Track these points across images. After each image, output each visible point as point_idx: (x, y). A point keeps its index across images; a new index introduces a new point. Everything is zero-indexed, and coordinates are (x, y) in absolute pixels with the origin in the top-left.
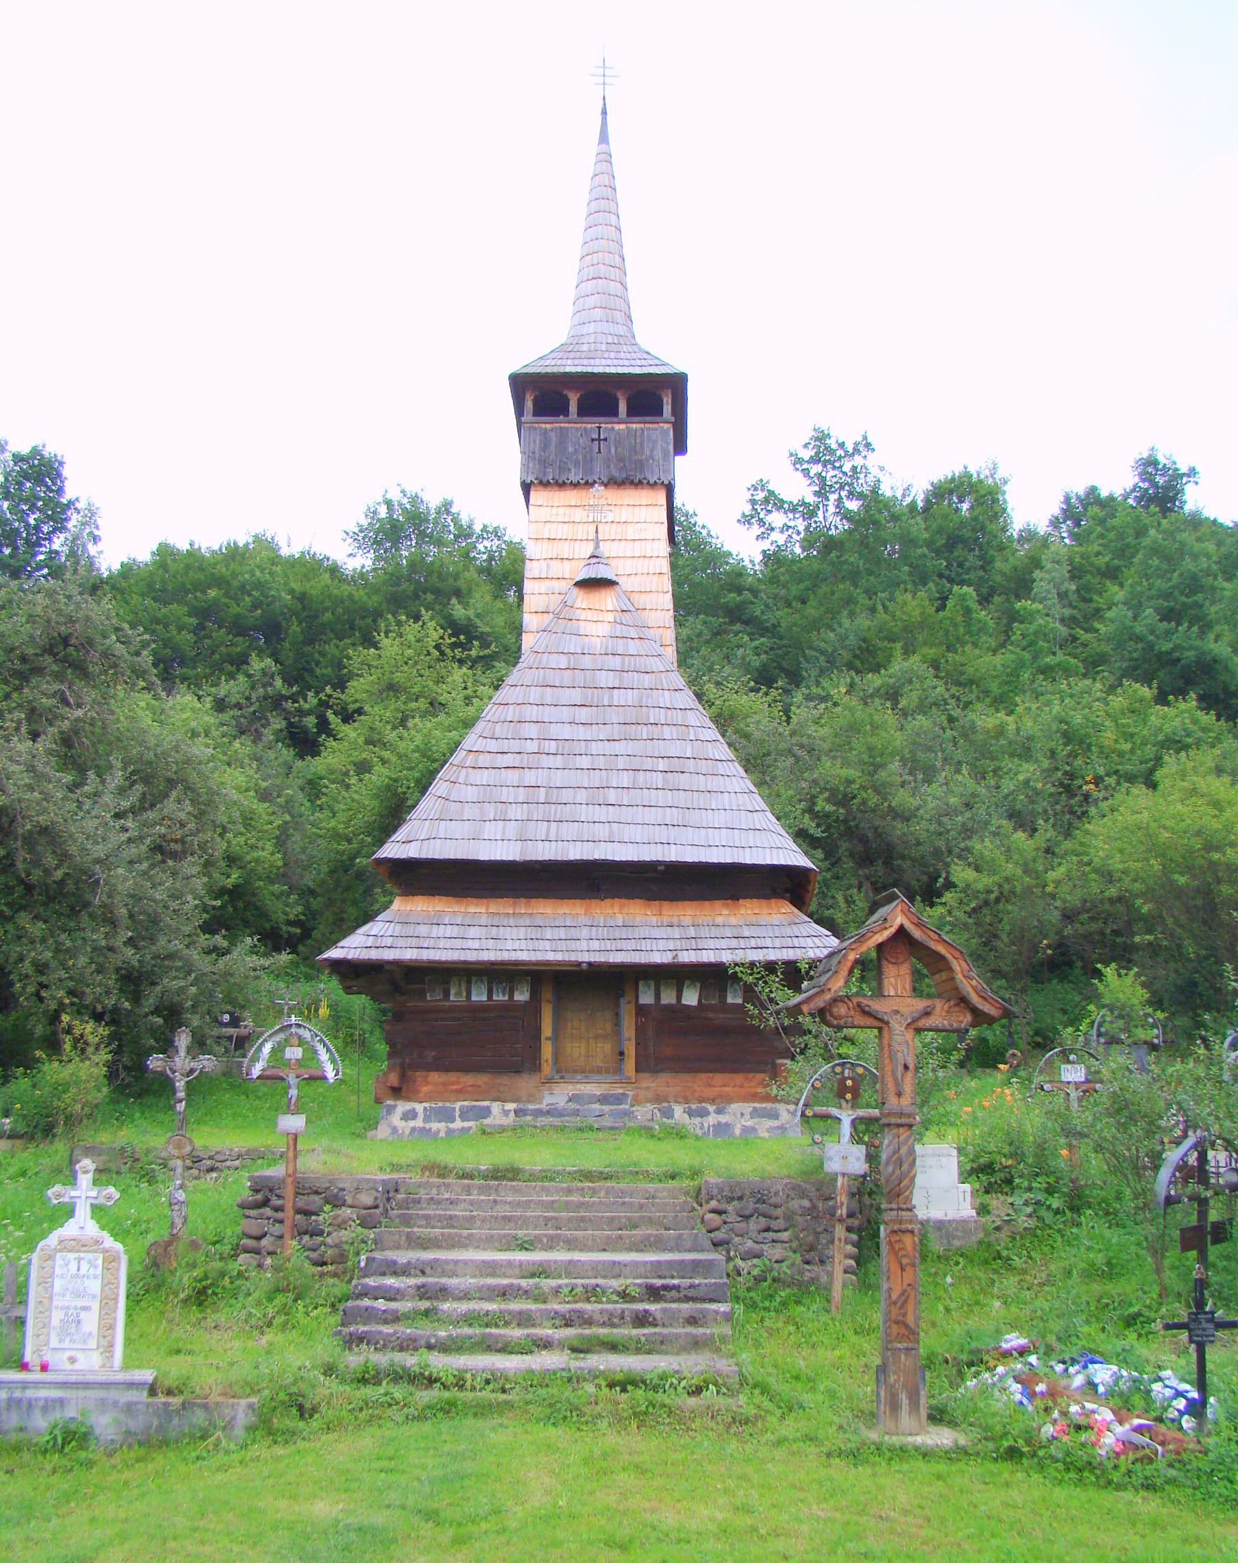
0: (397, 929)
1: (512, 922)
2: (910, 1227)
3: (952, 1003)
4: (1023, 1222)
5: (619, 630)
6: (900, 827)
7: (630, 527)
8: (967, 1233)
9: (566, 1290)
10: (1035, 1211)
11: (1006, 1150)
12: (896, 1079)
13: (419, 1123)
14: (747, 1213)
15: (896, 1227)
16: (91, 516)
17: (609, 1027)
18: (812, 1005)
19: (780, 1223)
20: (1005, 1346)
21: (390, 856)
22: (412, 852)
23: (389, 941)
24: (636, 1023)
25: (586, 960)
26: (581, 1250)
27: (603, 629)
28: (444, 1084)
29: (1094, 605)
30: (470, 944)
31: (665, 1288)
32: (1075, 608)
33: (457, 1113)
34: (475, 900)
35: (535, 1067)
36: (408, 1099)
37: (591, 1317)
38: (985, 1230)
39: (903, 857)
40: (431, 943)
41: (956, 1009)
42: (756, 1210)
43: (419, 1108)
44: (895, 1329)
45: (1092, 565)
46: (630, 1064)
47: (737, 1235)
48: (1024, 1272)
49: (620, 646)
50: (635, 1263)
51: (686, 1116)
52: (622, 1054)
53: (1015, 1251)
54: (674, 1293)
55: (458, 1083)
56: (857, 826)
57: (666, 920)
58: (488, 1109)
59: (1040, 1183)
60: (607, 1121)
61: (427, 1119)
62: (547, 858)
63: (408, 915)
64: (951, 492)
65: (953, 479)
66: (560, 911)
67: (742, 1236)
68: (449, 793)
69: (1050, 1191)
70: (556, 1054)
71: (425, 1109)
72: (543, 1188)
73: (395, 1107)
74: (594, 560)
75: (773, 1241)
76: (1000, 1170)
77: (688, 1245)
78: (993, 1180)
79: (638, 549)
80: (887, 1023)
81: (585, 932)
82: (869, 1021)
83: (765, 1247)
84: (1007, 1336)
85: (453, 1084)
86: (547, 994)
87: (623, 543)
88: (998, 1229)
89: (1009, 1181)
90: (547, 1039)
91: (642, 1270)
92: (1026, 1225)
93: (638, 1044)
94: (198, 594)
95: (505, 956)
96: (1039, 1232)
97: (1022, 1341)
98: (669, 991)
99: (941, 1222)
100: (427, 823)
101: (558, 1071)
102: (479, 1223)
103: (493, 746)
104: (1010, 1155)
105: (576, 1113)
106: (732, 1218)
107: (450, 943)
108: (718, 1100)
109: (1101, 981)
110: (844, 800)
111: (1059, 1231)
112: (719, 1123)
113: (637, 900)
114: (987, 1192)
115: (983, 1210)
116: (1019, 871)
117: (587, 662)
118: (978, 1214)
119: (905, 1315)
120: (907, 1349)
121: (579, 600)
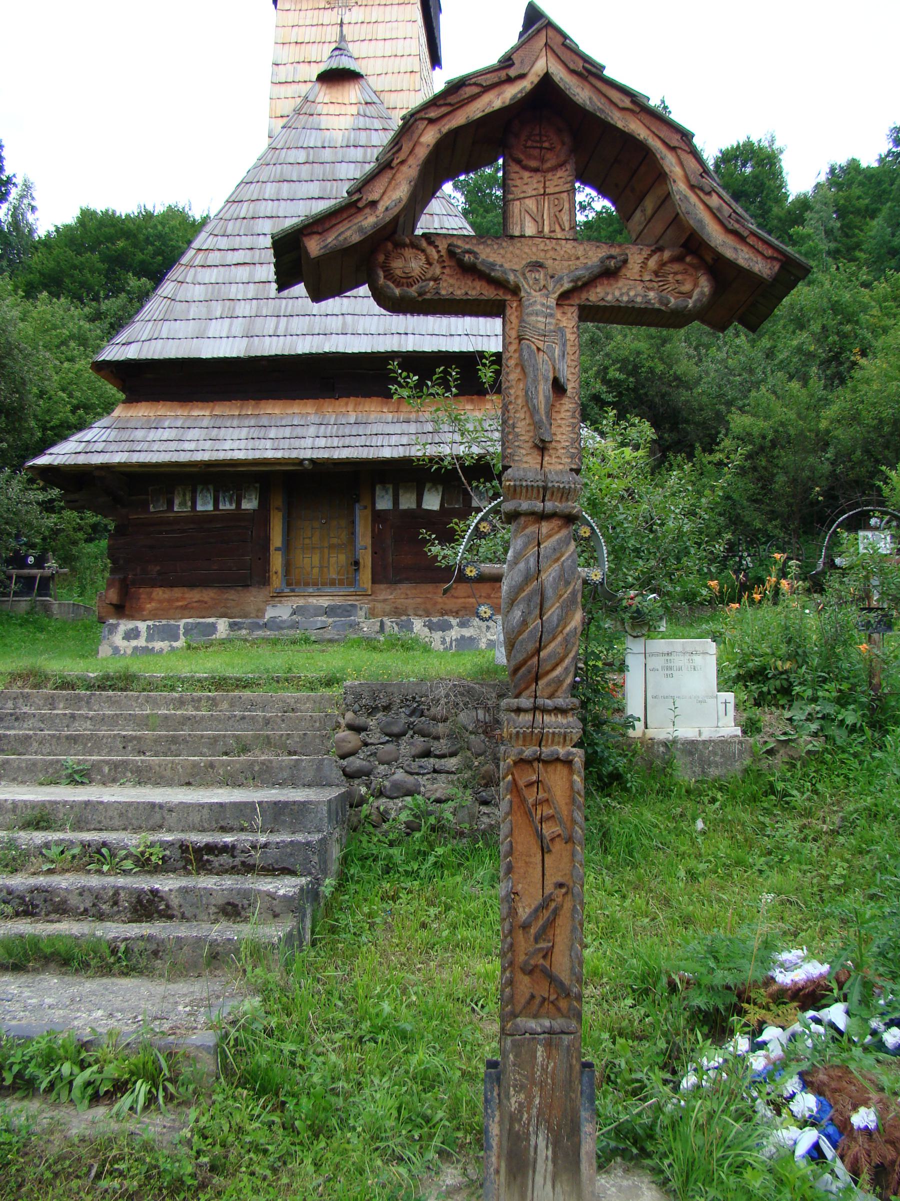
0: (113, 434)
1: (235, 423)
2: (562, 751)
3: (667, 255)
4: (806, 743)
5: (362, 122)
6: (684, 395)
7: (381, 27)
8: (729, 758)
9: (54, 851)
10: (822, 729)
11: (784, 649)
12: (532, 411)
13: (141, 642)
14: (396, 729)
15: (529, 752)
16: (27, 187)
17: (344, 536)
18: (331, 239)
19: (441, 746)
20: (784, 978)
21: (107, 359)
22: (132, 353)
23: (100, 446)
24: (373, 531)
25: (309, 457)
26: (157, 784)
27: (346, 122)
28: (169, 601)
29: (855, 240)
30: (187, 446)
31: (211, 849)
32: (839, 242)
33: (182, 631)
34: (200, 404)
35: (264, 580)
36: (132, 617)
37: (64, 901)
38: (753, 754)
39: (687, 421)
40: (145, 446)
41: (676, 267)
42: (410, 726)
43: (142, 626)
44: (525, 984)
45: (853, 206)
46: (366, 575)
47: (382, 763)
48: (808, 813)
49: (363, 138)
50: (185, 807)
51: (426, 630)
52: (357, 563)
53: (795, 783)
54: (225, 858)
55: (183, 598)
56: (646, 394)
57: (402, 417)
58: (213, 626)
59: (831, 690)
60: (330, 634)
61: (150, 638)
62: (273, 353)
63: (128, 421)
64: (736, 158)
65: (738, 146)
66: (290, 411)
67: (388, 763)
68: (175, 294)
69: (842, 701)
70: (288, 566)
71: (148, 627)
72: (148, 700)
73: (117, 625)
74: (337, 53)
75: (435, 771)
76: (774, 676)
77: (309, 776)
78: (765, 689)
79: (389, 48)
80: (515, 291)
81: (312, 430)
82: (476, 290)
83: (422, 780)
84: (785, 956)
85: (177, 600)
86: (277, 501)
87: (373, 42)
88: (771, 752)
89: (786, 691)
90: (277, 549)
91: (195, 818)
92: (810, 747)
93: (374, 553)
94: (109, 245)
95: (221, 456)
96: (828, 757)
97: (815, 969)
98: (408, 496)
99: (693, 743)
100: (150, 324)
101: (289, 584)
102: (35, 745)
103: (223, 243)
104: (789, 657)
105: (295, 626)
106: (375, 737)
107: (164, 447)
108: (461, 613)
109: (886, 483)
110: (634, 371)
111: (855, 755)
112: (463, 637)
113: (375, 399)
114: (757, 704)
115: (750, 727)
116: (794, 417)
117: (327, 155)
118: (744, 732)
119: (547, 954)
120: (551, 1032)
121: (322, 94)
